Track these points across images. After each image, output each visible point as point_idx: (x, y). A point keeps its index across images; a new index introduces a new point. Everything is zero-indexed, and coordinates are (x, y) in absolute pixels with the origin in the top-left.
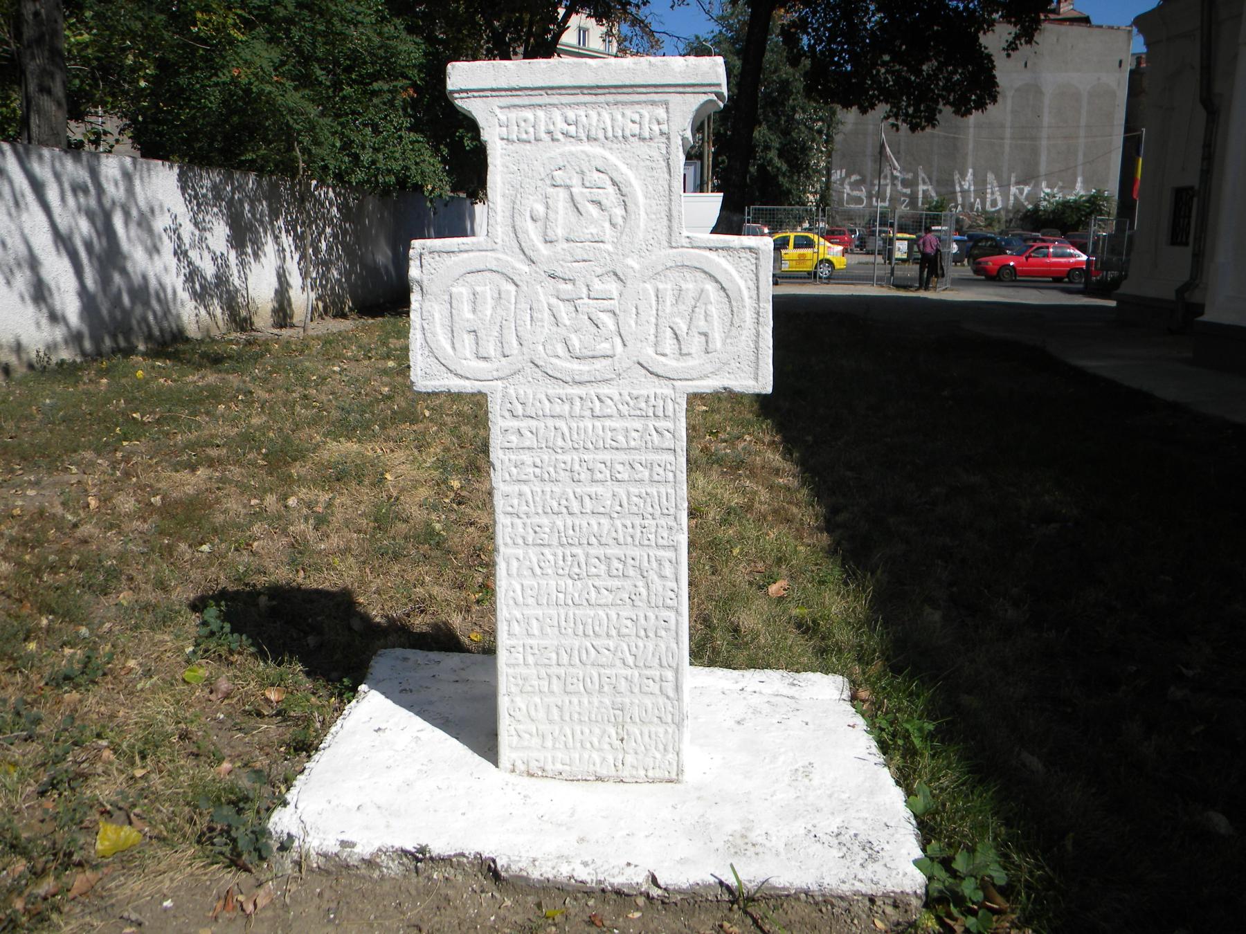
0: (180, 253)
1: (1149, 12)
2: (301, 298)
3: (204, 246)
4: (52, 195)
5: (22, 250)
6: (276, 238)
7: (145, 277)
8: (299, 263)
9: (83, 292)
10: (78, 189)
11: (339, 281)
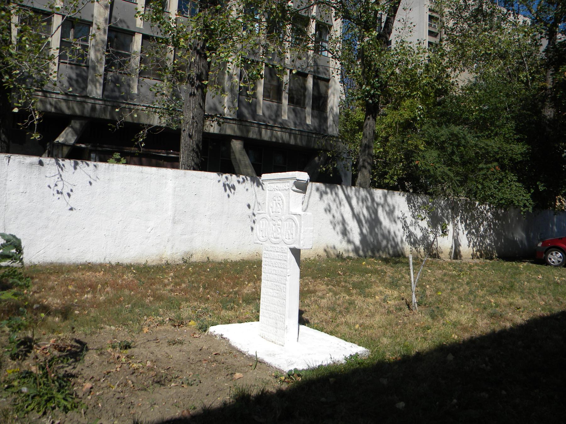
0: (405, 227)
1: (254, 168)
2: (466, 249)
3: (417, 225)
4: (354, 202)
5: (340, 218)
6: (455, 225)
7: (389, 232)
8: (467, 235)
9: (361, 233)
10: (364, 200)
11: (489, 245)
